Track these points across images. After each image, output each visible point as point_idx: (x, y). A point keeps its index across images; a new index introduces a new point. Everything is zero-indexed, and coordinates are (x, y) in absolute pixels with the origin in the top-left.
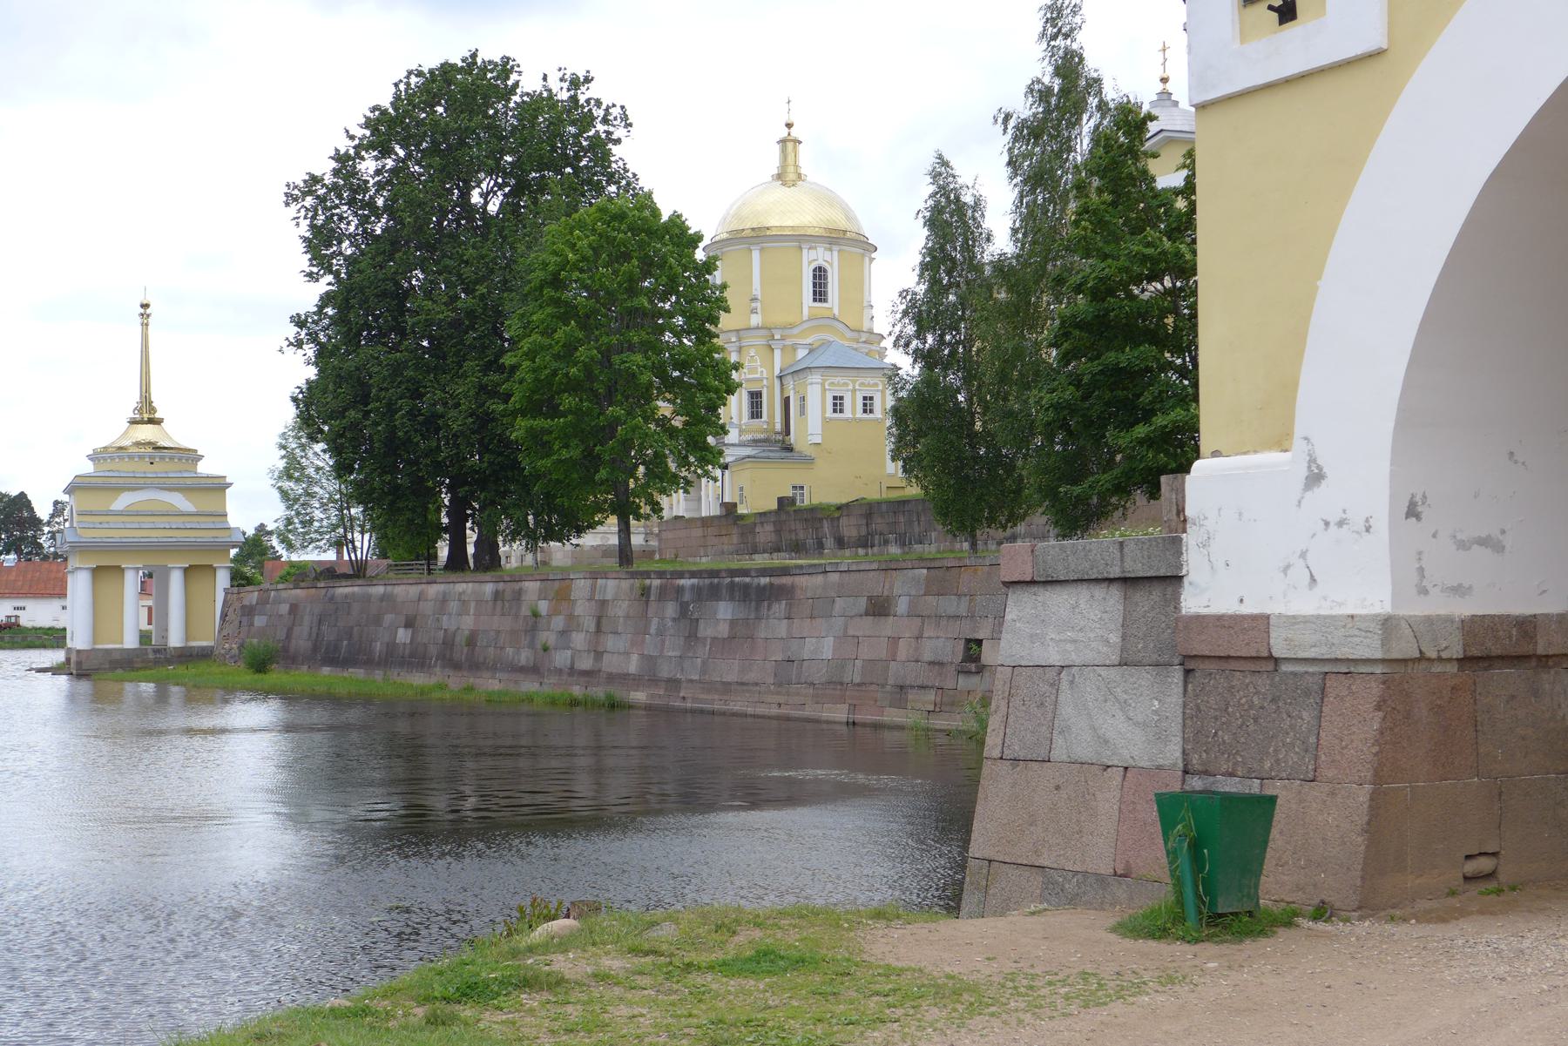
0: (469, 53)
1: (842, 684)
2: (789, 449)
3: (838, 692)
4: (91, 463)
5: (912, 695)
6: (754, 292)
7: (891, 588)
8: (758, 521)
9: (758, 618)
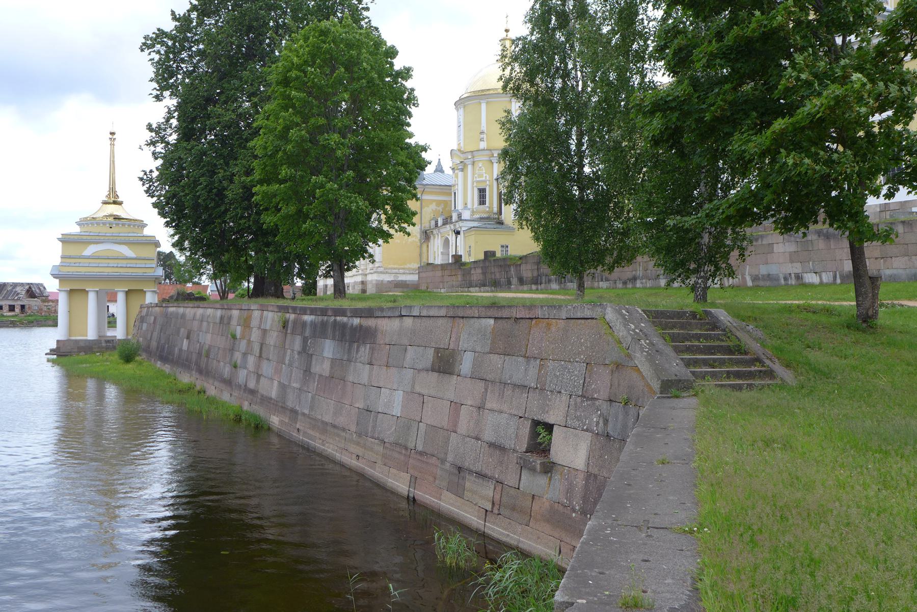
1: (406, 448)
3: (402, 458)
5: (470, 483)
7: (458, 339)
9: (349, 360)
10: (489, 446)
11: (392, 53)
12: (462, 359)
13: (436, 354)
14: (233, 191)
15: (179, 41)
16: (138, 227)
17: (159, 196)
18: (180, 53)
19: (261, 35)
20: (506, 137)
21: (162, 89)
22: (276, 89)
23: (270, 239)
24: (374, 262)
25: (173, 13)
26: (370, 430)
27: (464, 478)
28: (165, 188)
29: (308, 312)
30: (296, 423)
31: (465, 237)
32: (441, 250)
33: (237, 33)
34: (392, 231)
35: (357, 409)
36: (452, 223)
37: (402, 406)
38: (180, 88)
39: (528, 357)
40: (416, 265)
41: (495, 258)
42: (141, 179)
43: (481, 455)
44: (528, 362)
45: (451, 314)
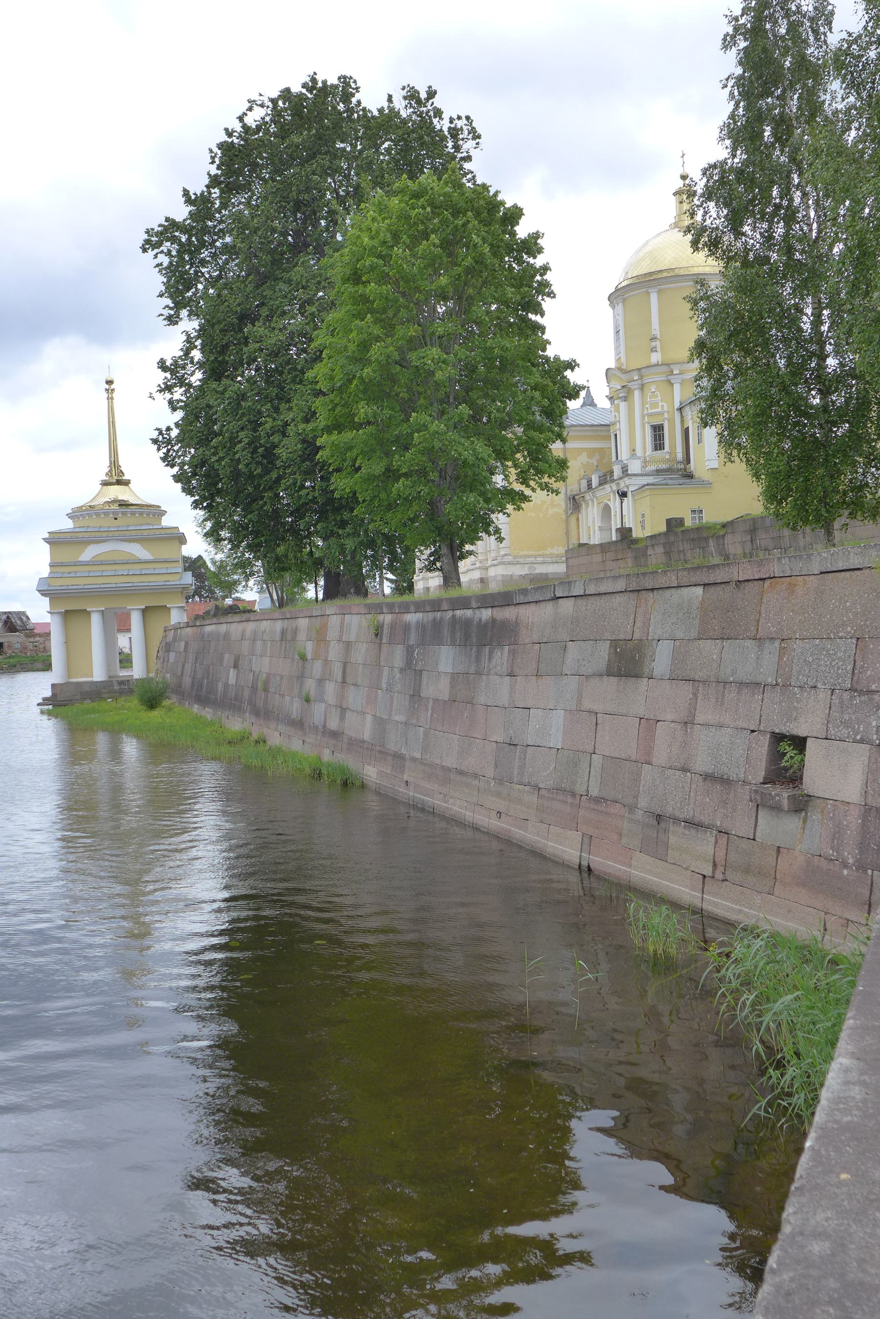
0: (309, 79)
1: (573, 795)
2: (690, 476)
4: (70, 521)
5: (676, 836)
6: (654, 332)
7: (647, 623)
8: (649, 543)
9: (478, 673)
10: (705, 780)
11: (515, 215)
12: (654, 654)
13: (612, 650)
14: (287, 449)
15: (197, 233)
16: (154, 515)
17: (183, 464)
18: (198, 251)
19: (312, 218)
20: (700, 322)
21: (178, 305)
22: (343, 288)
23: (346, 515)
24: (500, 540)
25: (186, 193)
26: (516, 773)
27: (666, 831)
28: (190, 452)
29: (412, 609)
30: (403, 774)
31: (634, 501)
32: (598, 523)
33: (279, 213)
34: (527, 492)
35: (494, 744)
36: (613, 481)
37: (564, 733)
38: (202, 303)
39: (760, 639)
40: (561, 550)
41: (683, 529)
42: (155, 441)
43: (692, 794)
44: (761, 647)
45: (634, 586)
